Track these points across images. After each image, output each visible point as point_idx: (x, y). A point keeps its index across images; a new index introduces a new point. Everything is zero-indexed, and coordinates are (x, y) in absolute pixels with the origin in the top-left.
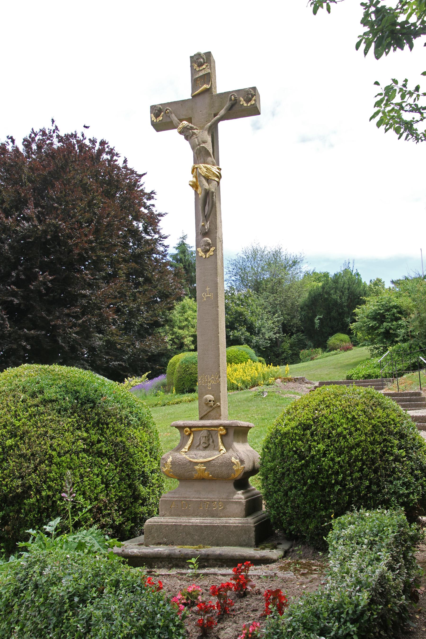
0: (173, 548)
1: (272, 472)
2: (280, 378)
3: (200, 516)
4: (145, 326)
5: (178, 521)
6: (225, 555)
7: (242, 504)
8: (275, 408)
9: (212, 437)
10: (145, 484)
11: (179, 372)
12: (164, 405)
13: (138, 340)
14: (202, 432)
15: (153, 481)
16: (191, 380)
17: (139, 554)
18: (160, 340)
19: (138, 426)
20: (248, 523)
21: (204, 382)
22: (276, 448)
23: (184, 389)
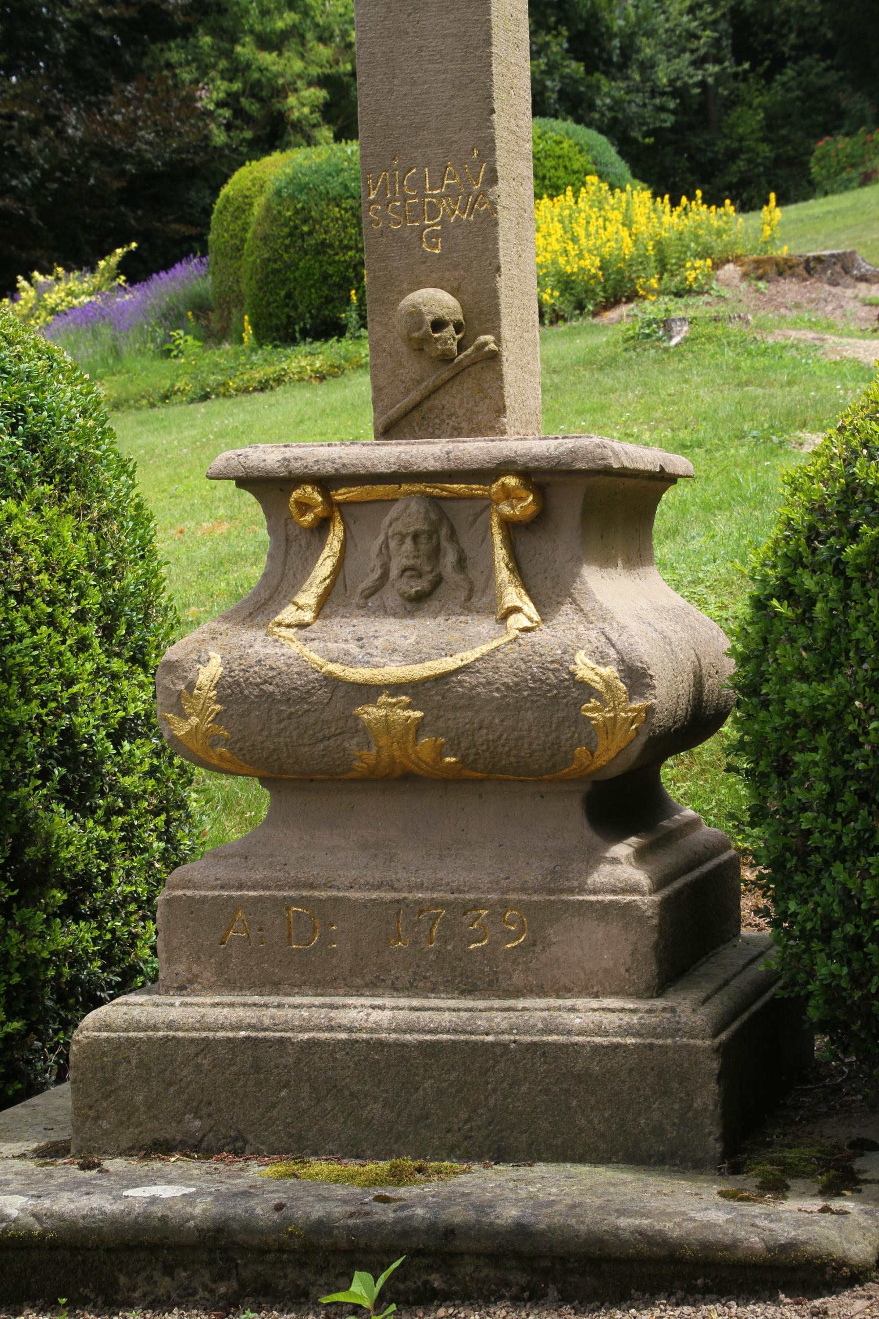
0: (241, 1183)
1: (822, 740)
2: (737, 260)
3: (396, 989)
4: (103, 33)
5: (268, 1016)
6: (551, 1230)
7: (641, 919)
8: (737, 394)
9: (453, 536)
10: (81, 798)
11: (265, 239)
12: (205, 397)
13: (75, 102)
14: (395, 510)
15: (126, 781)
16: (326, 277)
17: (37, 1228)
18: (176, 103)
19: (28, 481)
20: (675, 1032)
21: (401, 212)
22: (845, 597)
23: (291, 322)
